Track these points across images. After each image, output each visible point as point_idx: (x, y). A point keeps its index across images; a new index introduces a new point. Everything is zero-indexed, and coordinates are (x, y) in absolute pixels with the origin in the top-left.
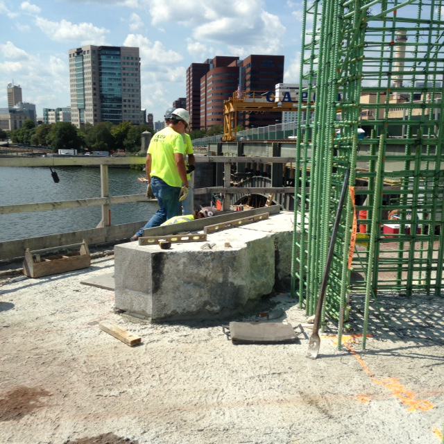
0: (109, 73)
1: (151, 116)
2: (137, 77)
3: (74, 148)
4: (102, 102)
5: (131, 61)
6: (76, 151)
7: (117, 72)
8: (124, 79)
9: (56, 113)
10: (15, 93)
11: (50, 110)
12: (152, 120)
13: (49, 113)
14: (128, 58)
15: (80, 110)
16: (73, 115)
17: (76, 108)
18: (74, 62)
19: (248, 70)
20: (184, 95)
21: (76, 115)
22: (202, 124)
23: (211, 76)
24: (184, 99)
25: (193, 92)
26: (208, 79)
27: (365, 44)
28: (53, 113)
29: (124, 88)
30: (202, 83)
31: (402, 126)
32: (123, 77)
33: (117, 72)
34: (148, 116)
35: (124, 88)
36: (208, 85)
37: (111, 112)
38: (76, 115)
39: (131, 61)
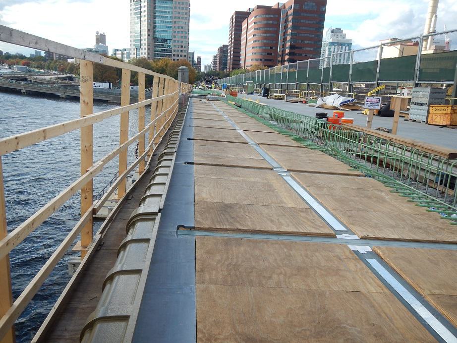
0: (162, 17)
1: (199, 58)
2: (187, 21)
3: (110, 81)
4: (155, 42)
5: (182, 6)
6: (111, 84)
7: (169, 16)
8: (175, 22)
9: (122, 52)
10: (101, 38)
11: (118, 50)
12: (200, 62)
13: (117, 52)
14: (179, 3)
15: (137, 49)
16: (131, 54)
17: (134, 47)
18: (134, 7)
19: (291, 12)
20: (227, 43)
21: (134, 54)
22: (242, 62)
23: (254, 18)
24: (227, 46)
25: (234, 48)
26: (249, 22)
27: (335, 46)
28: (120, 52)
29: (174, 29)
30: (244, 26)
31: (453, 80)
32: (174, 20)
33: (169, 16)
34: (197, 59)
35: (174, 29)
36: (248, 39)
37: (163, 51)
38: (134, 54)
39: (182, 6)
